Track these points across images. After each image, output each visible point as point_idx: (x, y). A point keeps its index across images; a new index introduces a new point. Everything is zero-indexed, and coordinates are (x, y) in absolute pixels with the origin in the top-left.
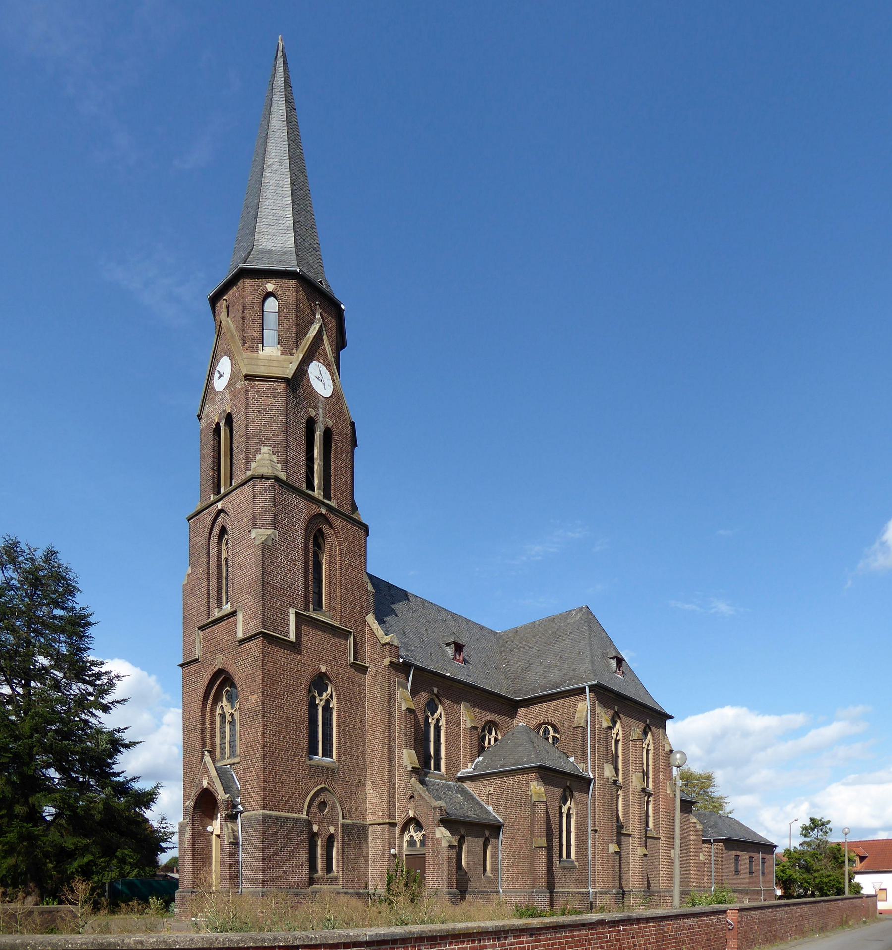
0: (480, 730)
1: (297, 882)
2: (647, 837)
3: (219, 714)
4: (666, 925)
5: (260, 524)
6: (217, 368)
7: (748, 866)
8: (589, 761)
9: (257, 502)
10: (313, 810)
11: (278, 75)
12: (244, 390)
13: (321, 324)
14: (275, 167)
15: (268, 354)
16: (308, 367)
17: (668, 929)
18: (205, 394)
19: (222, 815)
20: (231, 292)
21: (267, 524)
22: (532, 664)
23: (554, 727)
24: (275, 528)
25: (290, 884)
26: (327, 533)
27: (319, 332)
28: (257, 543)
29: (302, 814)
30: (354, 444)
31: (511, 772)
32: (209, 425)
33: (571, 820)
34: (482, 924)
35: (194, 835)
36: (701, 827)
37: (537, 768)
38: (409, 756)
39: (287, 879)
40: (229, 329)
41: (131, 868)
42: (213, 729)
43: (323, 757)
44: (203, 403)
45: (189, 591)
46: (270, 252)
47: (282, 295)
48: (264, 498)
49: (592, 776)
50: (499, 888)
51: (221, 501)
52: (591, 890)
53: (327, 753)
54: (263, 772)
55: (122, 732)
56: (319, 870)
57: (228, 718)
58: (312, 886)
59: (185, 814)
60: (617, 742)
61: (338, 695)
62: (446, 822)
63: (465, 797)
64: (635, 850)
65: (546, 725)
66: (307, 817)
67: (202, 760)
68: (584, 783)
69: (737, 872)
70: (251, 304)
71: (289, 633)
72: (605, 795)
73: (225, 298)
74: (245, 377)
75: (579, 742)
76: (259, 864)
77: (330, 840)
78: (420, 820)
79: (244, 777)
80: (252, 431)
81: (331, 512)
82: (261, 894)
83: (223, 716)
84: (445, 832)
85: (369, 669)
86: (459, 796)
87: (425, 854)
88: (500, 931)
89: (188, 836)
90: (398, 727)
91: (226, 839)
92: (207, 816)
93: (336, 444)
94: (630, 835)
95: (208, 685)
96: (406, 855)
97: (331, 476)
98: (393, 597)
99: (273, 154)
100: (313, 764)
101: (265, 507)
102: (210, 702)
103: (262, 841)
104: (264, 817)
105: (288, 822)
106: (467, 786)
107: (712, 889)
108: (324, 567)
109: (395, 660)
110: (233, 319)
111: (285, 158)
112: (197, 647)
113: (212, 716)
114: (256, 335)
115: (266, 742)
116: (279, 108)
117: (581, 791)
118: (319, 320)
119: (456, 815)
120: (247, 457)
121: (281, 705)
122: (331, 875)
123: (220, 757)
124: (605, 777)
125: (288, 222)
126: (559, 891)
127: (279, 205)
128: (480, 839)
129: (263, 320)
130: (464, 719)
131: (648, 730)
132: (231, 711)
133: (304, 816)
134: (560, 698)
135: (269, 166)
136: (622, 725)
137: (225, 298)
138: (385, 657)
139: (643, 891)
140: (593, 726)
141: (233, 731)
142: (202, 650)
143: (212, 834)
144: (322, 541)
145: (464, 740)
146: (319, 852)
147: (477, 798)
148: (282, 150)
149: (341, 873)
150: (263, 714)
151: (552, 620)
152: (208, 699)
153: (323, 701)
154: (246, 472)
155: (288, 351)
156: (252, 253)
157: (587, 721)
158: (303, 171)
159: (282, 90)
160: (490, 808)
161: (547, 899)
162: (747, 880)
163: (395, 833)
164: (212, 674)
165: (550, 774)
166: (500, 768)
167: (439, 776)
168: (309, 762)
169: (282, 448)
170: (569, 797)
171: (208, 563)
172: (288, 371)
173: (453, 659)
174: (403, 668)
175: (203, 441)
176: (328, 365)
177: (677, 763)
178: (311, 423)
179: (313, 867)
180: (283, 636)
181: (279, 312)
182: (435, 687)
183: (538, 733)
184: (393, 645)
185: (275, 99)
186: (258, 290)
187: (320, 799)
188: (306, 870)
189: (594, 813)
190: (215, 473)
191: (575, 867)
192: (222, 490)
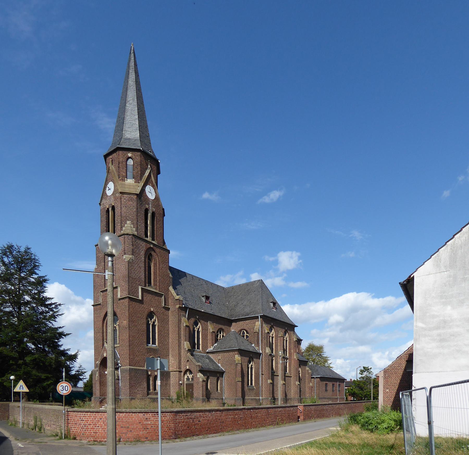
0: (216, 332)
2: (285, 376)
7: (331, 388)
11: (131, 61)
12: (120, 197)
14: (131, 102)
17: (271, 411)
23: (246, 331)
24: (133, 255)
30: (164, 215)
32: (104, 208)
33: (252, 370)
34: (205, 408)
38: (187, 344)
40: (113, 171)
43: (152, 344)
46: (129, 139)
49: (261, 352)
53: (154, 343)
55: (61, 328)
59: (96, 366)
60: (272, 338)
61: (158, 320)
62: (201, 371)
63: (210, 360)
64: (280, 382)
69: (326, 390)
72: (266, 360)
75: (256, 338)
86: (207, 360)
87: (193, 384)
89: (97, 375)
90: (182, 333)
93: (157, 218)
99: (130, 96)
104: (130, 369)
106: (211, 356)
109: (181, 306)
111: (135, 98)
119: (205, 368)
120: (121, 225)
122: (156, 391)
124: (266, 352)
125: (137, 126)
127: (133, 119)
129: (127, 168)
131: (286, 332)
133: (145, 368)
135: (128, 101)
136: (275, 331)
138: (177, 304)
140: (262, 332)
144: (151, 258)
145: (209, 337)
146: (151, 382)
157: (259, 330)
159: (133, 68)
160: (220, 365)
161: (242, 402)
166: (223, 349)
167: (199, 352)
168: (147, 347)
169: (135, 222)
170: (251, 360)
171: (105, 265)
174: (184, 309)
176: (153, 186)
178: (146, 211)
179: (148, 389)
181: (133, 165)
183: (240, 334)
185: (131, 72)
191: (254, 389)
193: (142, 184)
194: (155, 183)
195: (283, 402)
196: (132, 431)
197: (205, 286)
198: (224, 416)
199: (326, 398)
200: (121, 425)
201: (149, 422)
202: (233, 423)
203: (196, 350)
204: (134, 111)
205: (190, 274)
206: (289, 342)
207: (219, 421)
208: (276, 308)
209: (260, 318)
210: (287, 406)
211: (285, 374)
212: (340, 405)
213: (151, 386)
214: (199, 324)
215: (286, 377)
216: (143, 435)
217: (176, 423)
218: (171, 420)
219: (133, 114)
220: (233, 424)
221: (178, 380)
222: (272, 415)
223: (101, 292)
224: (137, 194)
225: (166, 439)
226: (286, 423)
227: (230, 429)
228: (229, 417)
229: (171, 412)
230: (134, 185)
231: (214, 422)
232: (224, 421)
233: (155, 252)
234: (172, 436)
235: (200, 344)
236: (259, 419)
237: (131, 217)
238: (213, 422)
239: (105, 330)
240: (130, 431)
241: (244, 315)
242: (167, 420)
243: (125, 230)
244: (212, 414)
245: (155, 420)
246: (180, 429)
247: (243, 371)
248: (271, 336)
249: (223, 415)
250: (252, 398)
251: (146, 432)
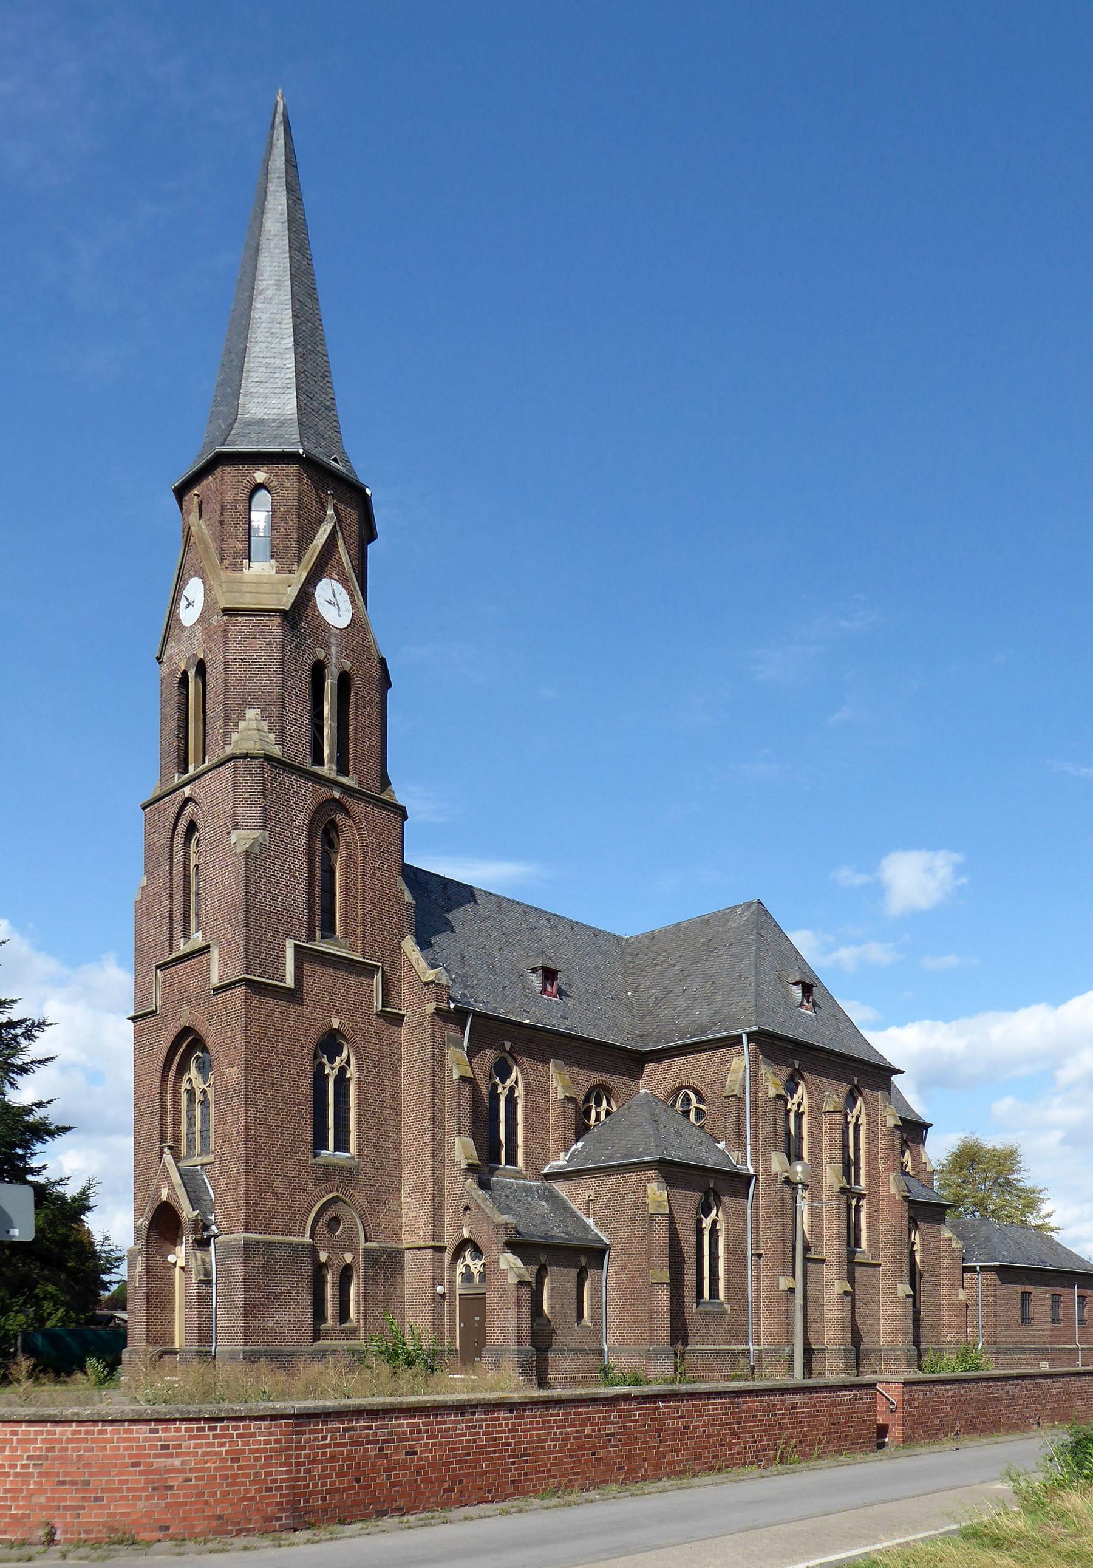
0: (580, 1101)
1: (295, 1336)
2: (852, 1263)
3: (186, 1090)
4: (744, 1402)
6: (185, 593)
7: (1048, 1309)
8: (749, 1147)
10: (318, 1230)
13: (335, 523)
14: (270, 293)
15: (257, 574)
16: (315, 589)
18: (167, 627)
19: (188, 1240)
20: (205, 483)
21: (254, 823)
23: (697, 1093)
24: (264, 827)
25: (285, 1339)
26: (342, 825)
27: (332, 537)
28: (239, 850)
29: (303, 1236)
30: (389, 684)
31: (620, 1168)
32: (172, 673)
34: (437, 1398)
35: (148, 1269)
36: (960, 1246)
38: (464, 1145)
39: (279, 1333)
40: (202, 539)
41: (54, 1306)
42: (176, 1112)
43: (335, 1151)
45: (144, 910)
46: (261, 422)
49: (752, 1172)
50: (604, 1343)
51: (189, 786)
52: (752, 1348)
53: (342, 1144)
54: (246, 1178)
56: (329, 1318)
57: (199, 1097)
58: (318, 1343)
60: (799, 1116)
61: (359, 1059)
62: (515, 1246)
63: (553, 1205)
65: (687, 1091)
66: (311, 1240)
67: (161, 1158)
68: (739, 1182)
69: (1026, 1319)
71: (285, 976)
74: (223, 612)
75: (732, 1120)
76: (240, 1311)
77: (346, 1275)
78: (479, 1242)
79: (220, 1185)
81: (347, 794)
82: (241, 1354)
83: (191, 1093)
84: (513, 1261)
86: (543, 1203)
87: (485, 1294)
88: (464, 1406)
89: (140, 1270)
91: (193, 1276)
92: (167, 1239)
93: (356, 694)
94: (823, 1261)
95: (170, 1050)
96: (460, 1295)
97: (349, 740)
98: (450, 900)
99: (267, 274)
100: (320, 1163)
102: (172, 1073)
103: (244, 1279)
104: (247, 1242)
105: (283, 1250)
106: (558, 1187)
107: (980, 1346)
108: (337, 874)
109: (442, 1005)
110: (208, 523)
111: (285, 278)
112: (154, 994)
114: (239, 546)
115: (250, 1135)
116: (277, 202)
117: (734, 1194)
118: (331, 517)
119: (532, 1236)
120: (226, 725)
121: (273, 1080)
122: (347, 1325)
123: (187, 1152)
124: (773, 1173)
126: (695, 1350)
128: (572, 1269)
130: (555, 1085)
131: (856, 1093)
133: (307, 1239)
138: (428, 1001)
139: (844, 1350)
141: (205, 1115)
142: (162, 998)
143: (175, 1267)
144: (336, 836)
145: (554, 1118)
146: (329, 1291)
147: (572, 1206)
148: (280, 267)
150: (246, 1094)
151: (705, 921)
152: (170, 1069)
153: (336, 1070)
155: (285, 568)
156: (236, 425)
157: (744, 1087)
160: (590, 1222)
162: (1049, 1332)
163: (444, 1262)
165: (680, 1170)
166: (604, 1161)
168: (314, 1161)
169: (275, 710)
170: (713, 1203)
171: (171, 873)
172: (285, 599)
173: (541, 993)
174: (454, 1016)
175: (164, 695)
176: (344, 581)
177: (798, 1178)
178: (318, 670)
179: (319, 1314)
180: (276, 980)
182: (507, 1040)
183: (673, 1105)
184: (439, 984)
187: (330, 1213)
188: (308, 1318)
190: (181, 743)
191: (724, 1312)
193: (301, 575)
194: (352, 570)
195: (846, 1363)
196: (102, 1499)
197: (546, 932)
198: (528, 1430)
199: (1024, 1349)
200: (57, 1475)
201: (177, 1462)
202: (571, 1456)
203: (503, 1169)
204: (280, 323)
205: (491, 894)
206: (868, 1133)
207: (507, 1451)
208: (815, 1005)
209: (748, 1043)
210: (827, 1387)
211: (851, 1254)
212: (1073, 1378)
213: (329, 1305)
214: (514, 1071)
215: (809, 1264)
216: (149, 1514)
217: (298, 1464)
218: (272, 1450)
219: (277, 335)
220: (574, 1462)
221: (430, 1283)
222: (755, 1421)
223: (157, 967)
224: (282, 613)
225: (248, 1530)
226: (823, 1453)
227: (559, 1482)
228: (555, 1434)
229: (273, 1418)
230: (274, 582)
231: (481, 1453)
232: (531, 1448)
233: (348, 814)
234: (281, 1518)
235: (348, 1132)
236: (693, 1438)
237: (260, 693)
238: (475, 1454)
239: (169, 1103)
240: (96, 1499)
241: (688, 1032)
242: (257, 1451)
243: (237, 741)
244: (471, 1421)
245: (200, 1451)
246: (316, 1486)
247: (679, 1245)
248: (795, 1108)
249: (526, 1424)
250: (717, 1347)
251: (162, 1503)
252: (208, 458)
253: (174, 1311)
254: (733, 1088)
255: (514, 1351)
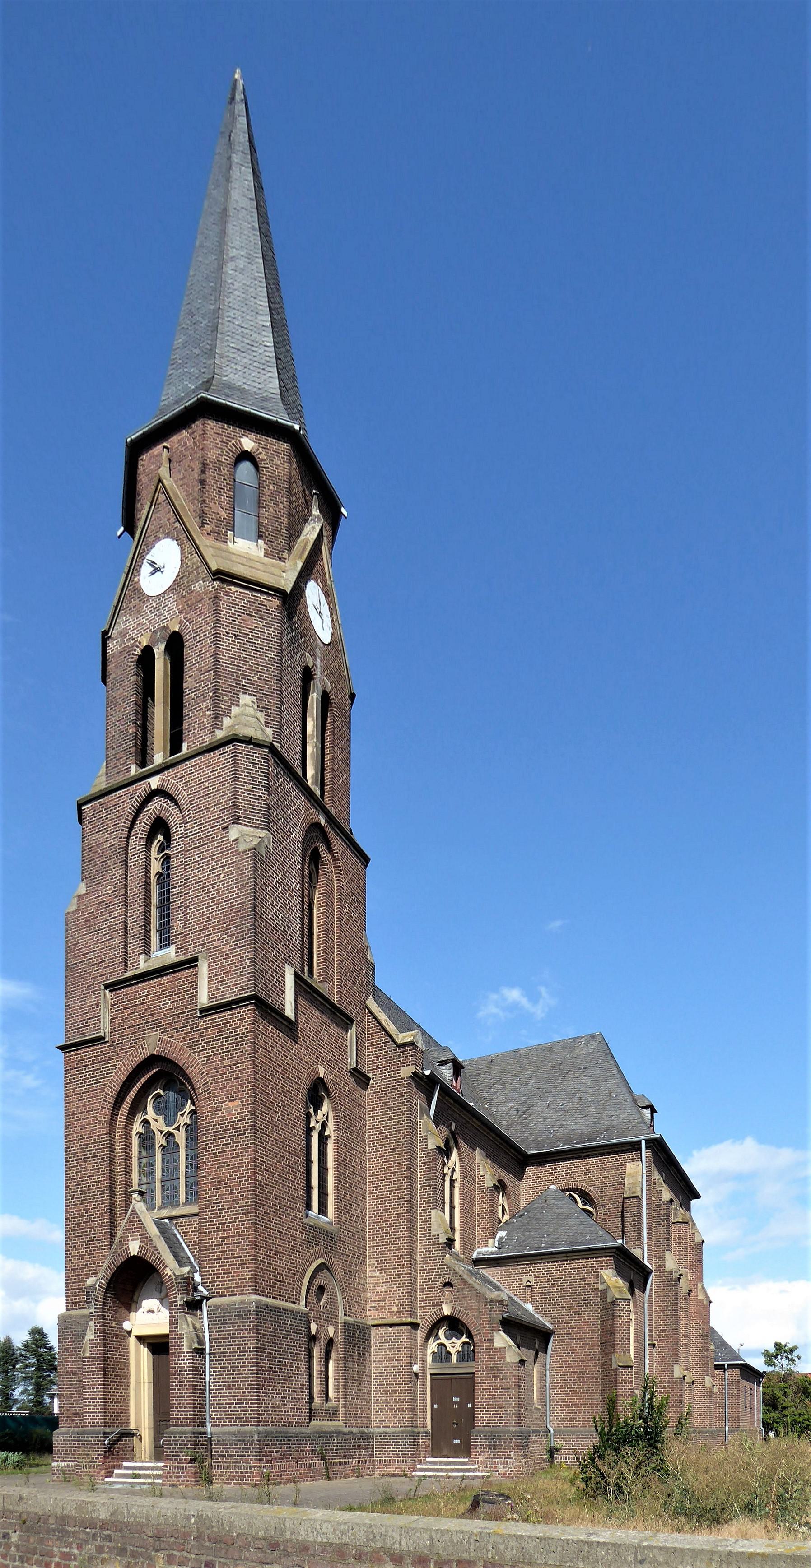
5: (245, 818)
9: (241, 782)
20: (175, 438)
22: (533, 1106)
24: (268, 829)
28: (242, 847)
37: (614, 1250)
39: (285, 1412)
44: (115, 612)
47: (268, 462)
48: (252, 777)
53: (323, 1210)
56: (315, 1397)
57: (160, 1140)
65: (572, 1193)
70: (216, 463)
72: (667, 1295)
73: (165, 444)
80: (224, 665)
81: (330, 825)
83: (146, 1139)
85: (371, 1082)
87: (473, 1373)
89: (92, 1337)
91: (185, 1343)
92: (122, 1303)
95: (124, 1083)
96: (431, 1375)
100: (312, 1224)
101: (253, 791)
104: (259, 1306)
106: (488, 1272)
110: (181, 482)
113: (127, 1135)
114: (223, 514)
120: (216, 707)
130: (481, 1173)
132: (166, 1129)
133: (302, 1307)
134: (596, 1154)
137: (165, 444)
138: (404, 1064)
149: (341, 1401)
152: (120, 1107)
154: (214, 732)
158: (277, 284)
160: (529, 1307)
164: (135, 1064)
166: (543, 1248)
168: (305, 1221)
169: (273, 702)
178: (307, 675)
184: (417, 1047)
186: (227, 443)
187: (318, 1281)
189: (651, 1320)
192: (159, 758)
223: (107, 987)
224: (279, 592)
237: (256, 679)
252: (187, 404)
253: (128, 1386)
254: (634, 1190)
255: (515, 1432)
